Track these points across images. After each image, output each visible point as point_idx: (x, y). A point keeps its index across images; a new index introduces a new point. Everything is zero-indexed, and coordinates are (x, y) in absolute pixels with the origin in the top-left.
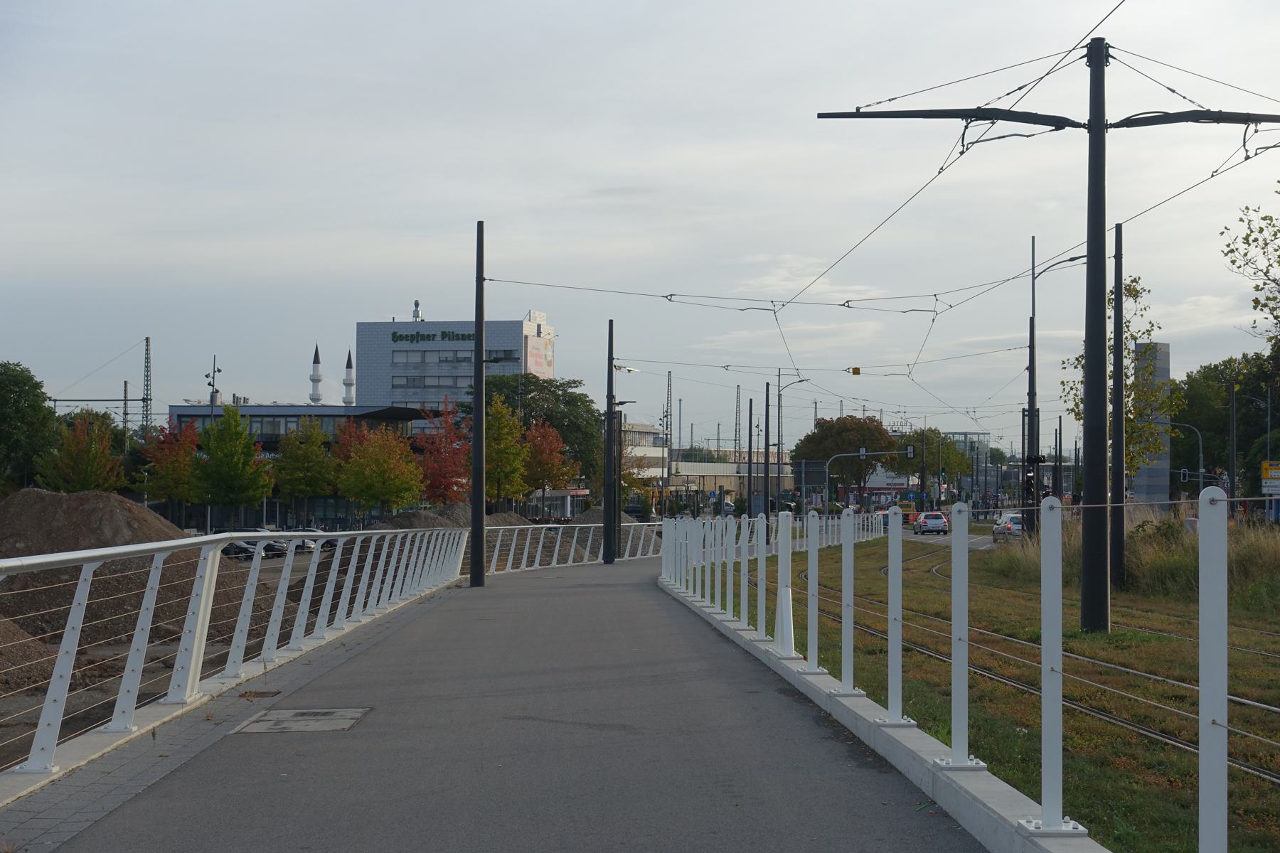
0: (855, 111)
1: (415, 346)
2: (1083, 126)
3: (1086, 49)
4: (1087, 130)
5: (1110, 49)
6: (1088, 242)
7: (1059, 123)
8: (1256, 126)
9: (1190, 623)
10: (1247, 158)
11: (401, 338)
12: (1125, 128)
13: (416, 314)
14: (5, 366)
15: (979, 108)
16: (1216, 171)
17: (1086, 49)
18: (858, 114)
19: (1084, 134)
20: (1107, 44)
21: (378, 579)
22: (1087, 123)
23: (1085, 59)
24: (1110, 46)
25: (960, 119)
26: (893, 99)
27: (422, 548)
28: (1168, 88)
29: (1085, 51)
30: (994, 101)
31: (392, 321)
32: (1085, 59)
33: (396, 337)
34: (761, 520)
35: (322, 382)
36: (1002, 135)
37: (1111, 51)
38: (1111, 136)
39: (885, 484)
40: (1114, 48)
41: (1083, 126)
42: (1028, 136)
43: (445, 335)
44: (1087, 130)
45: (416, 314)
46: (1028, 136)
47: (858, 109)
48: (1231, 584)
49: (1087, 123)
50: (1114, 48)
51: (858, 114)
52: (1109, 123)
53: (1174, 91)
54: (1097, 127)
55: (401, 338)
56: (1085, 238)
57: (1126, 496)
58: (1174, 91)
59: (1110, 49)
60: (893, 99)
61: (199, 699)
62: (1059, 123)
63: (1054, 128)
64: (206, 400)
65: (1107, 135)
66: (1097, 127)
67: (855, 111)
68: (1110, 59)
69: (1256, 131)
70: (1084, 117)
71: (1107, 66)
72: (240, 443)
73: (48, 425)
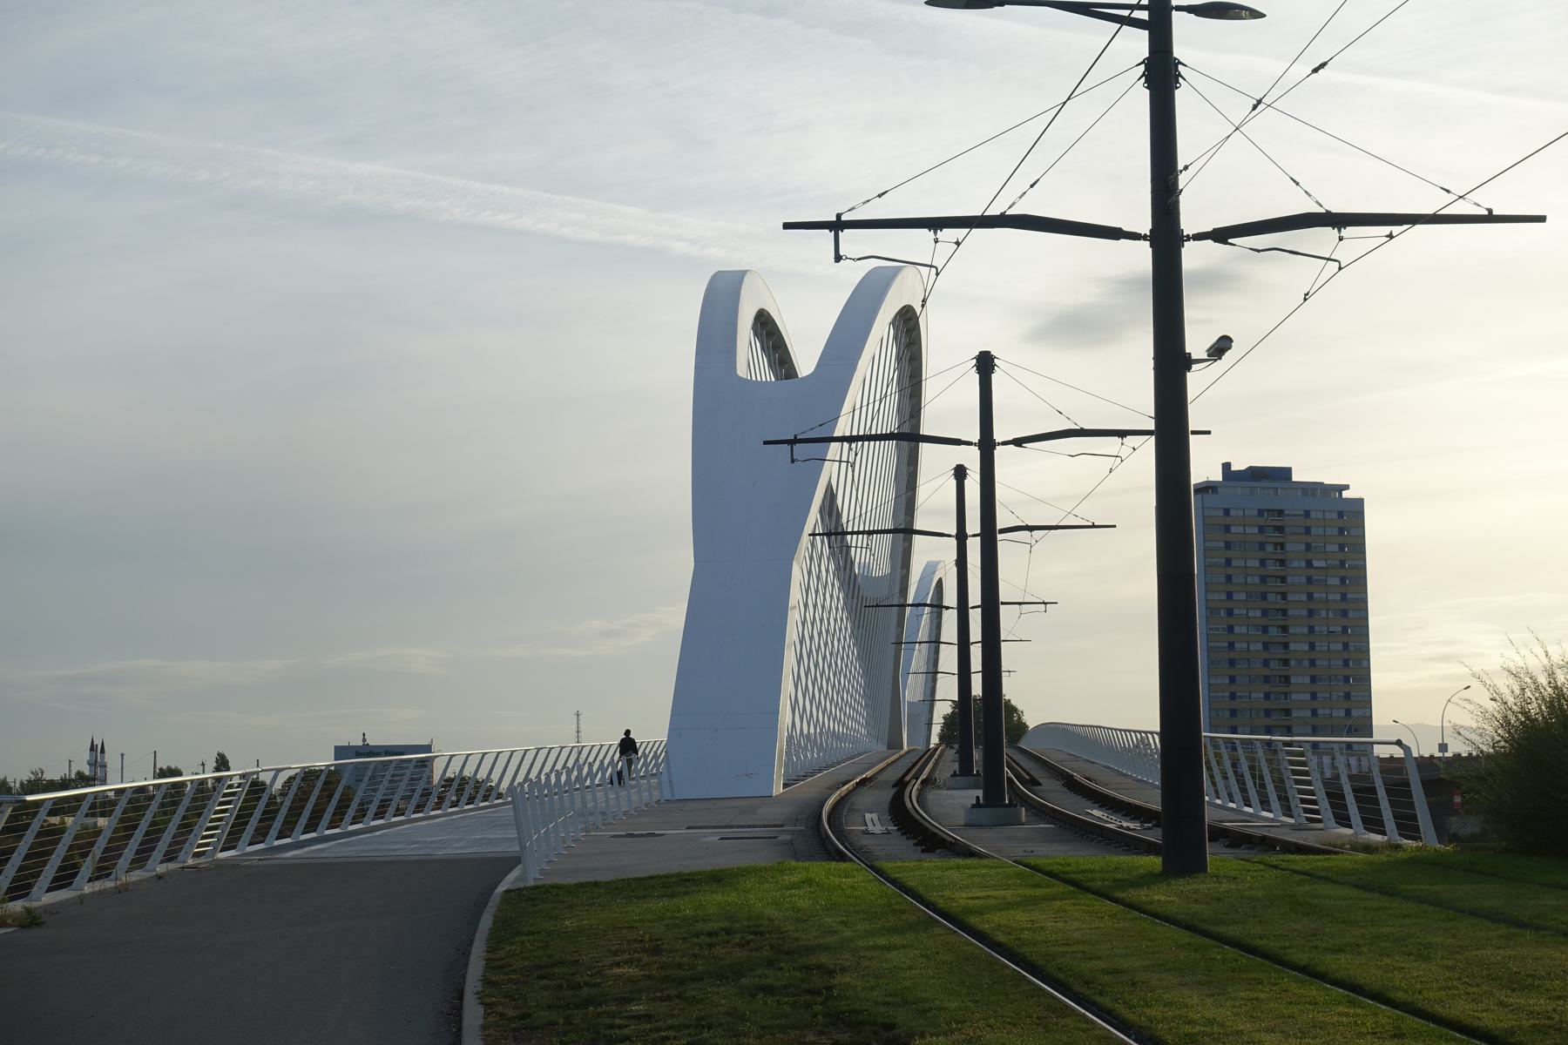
0: (835, 219)
2: (1144, 238)
3: (1143, 65)
4: (1148, 243)
5: (1180, 66)
13: (364, 740)
14: (17, 775)
17: (1143, 65)
20: (1176, 59)
22: (1148, 234)
24: (1180, 63)
25: (926, 230)
26: (1294, 181)
27: (1038, 890)
34: (482, 775)
36: (1292, 255)
39: (1479, 668)
40: (1186, 66)
41: (1144, 238)
45: (364, 740)
47: (839, 216)
49: (1148, 234)
50: (1186, 66)
52: (1185, 234)
59: (1180, 66)
60: (1294, 181)
62: (954, 674)
65: (1183, 250)
67: (835, 219)
69: (1341, 239)
71: (1177, 88)
72: (1140, 925)
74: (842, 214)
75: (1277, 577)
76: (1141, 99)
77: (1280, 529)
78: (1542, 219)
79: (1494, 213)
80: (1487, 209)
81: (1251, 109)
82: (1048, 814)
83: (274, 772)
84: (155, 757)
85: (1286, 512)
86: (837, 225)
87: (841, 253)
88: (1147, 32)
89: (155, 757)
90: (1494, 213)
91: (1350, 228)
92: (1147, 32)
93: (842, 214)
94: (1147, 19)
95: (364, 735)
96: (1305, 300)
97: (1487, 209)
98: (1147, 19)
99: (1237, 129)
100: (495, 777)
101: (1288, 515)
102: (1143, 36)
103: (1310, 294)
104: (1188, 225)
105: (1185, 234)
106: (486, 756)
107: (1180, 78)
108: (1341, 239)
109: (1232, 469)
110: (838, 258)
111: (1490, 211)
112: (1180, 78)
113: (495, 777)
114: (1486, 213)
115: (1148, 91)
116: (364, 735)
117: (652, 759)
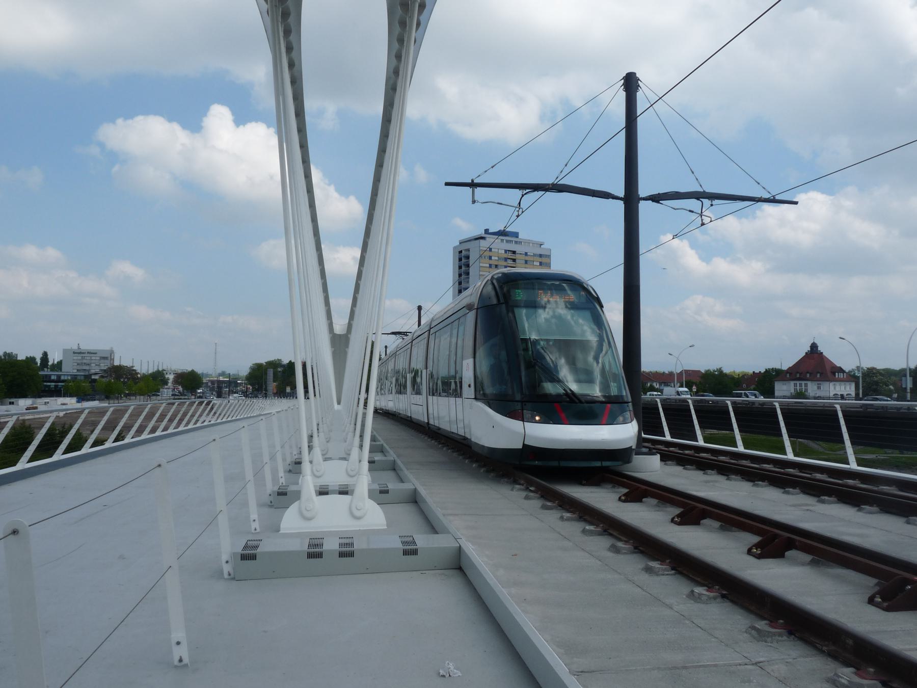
1: (80, 355)
4: (623, 202)
6: (624, 263)
8: (712, 202)
9: (844, 448)
10: (703, 224)
11: (76, 353)
16: (676, 235)
19: (621, 205)
21: (49, 422)
24: (639, 79)
33: (74, 353)
35: (115, 349)
43: (88, 353)
44: (623, 202)
47: (472, 181)
54: (631, 200)
55: (76, 353)
56: (622, 261)
61: (238, 403)
64: (713, 201)
66: (631, 200)
69: (712, 205)
75: (511, 259)
76: (622, 95)
77: (514, 260)
79: (475, 182)
81: (157, 465)
85: (517, 252)
86: (473, 185)
87: (476, 199)
90: (475, 182)
91: (639, 191)
95: (79, 344)
96: (673, 239)
101: (518, 254)
103: (678, 235)
107: (639, 81)
108: (712, 205)
109: (623, 197)
110: (474, 202)
111: (472, 181)
112: (639, 81)
115: (625, 93)
116: (79, 344)
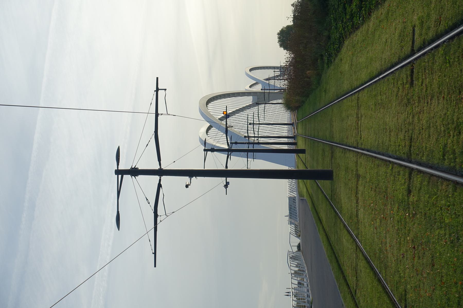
2: (160, 178)
3: (132, 177)
7: (160, 186)
8: (158, 216)
12: (161, 162)
13: (287, 216)
14: (291, 302)
15: (154, 213)
17: (132, 177)
18: (155, 253)
19: (163, 178)
20: (131, 168)
23: (136, 177)
24: (132, 167)
25: (158, 218)
28: (146, 147)
29: (133, 177)
30: (151, 247)
31: (254, 153)
32: (136, 177)
37: (133, 167)
38: (164, 167)
41: (160, 178)
42: (164, 196)
45: (287, 216)
46: (164, 196)
47: (153, 253)
48: (427, 52)
51: (155, 253)
52: (160, 168)
53: (147, 145)
54: (161, 172)
57: (361, 163)
58: (147, 145)
62: (160, 186)
63: (161, 188)
66: (161, 172)
68: (136, 167)
70: (157, 177)
71: (138, 168)
73: (324, 59)
74: (153, 252)
78: (157, 78)
79: (156, 90)
80: (155, 92)
82: (351, 268)
83: (291, 234)
84: (288, 288)
88: (124, 175)
89: (288, 288)
90: (156, 90)
92: (124, 175)
93: (153, 252)
94: (121, 175)
95: (285, 216)
97: (155, 92)
98: (121, 175)
99: (254, 124)
100: (286, 129)
102: (125, 176)
104: (157, 167)
105: (160, 168)
106: (293, 283)
111: (155, 91)
113: (286, 129)
114: (155, 92)
116: (285, 216)
117: (294, 254)
